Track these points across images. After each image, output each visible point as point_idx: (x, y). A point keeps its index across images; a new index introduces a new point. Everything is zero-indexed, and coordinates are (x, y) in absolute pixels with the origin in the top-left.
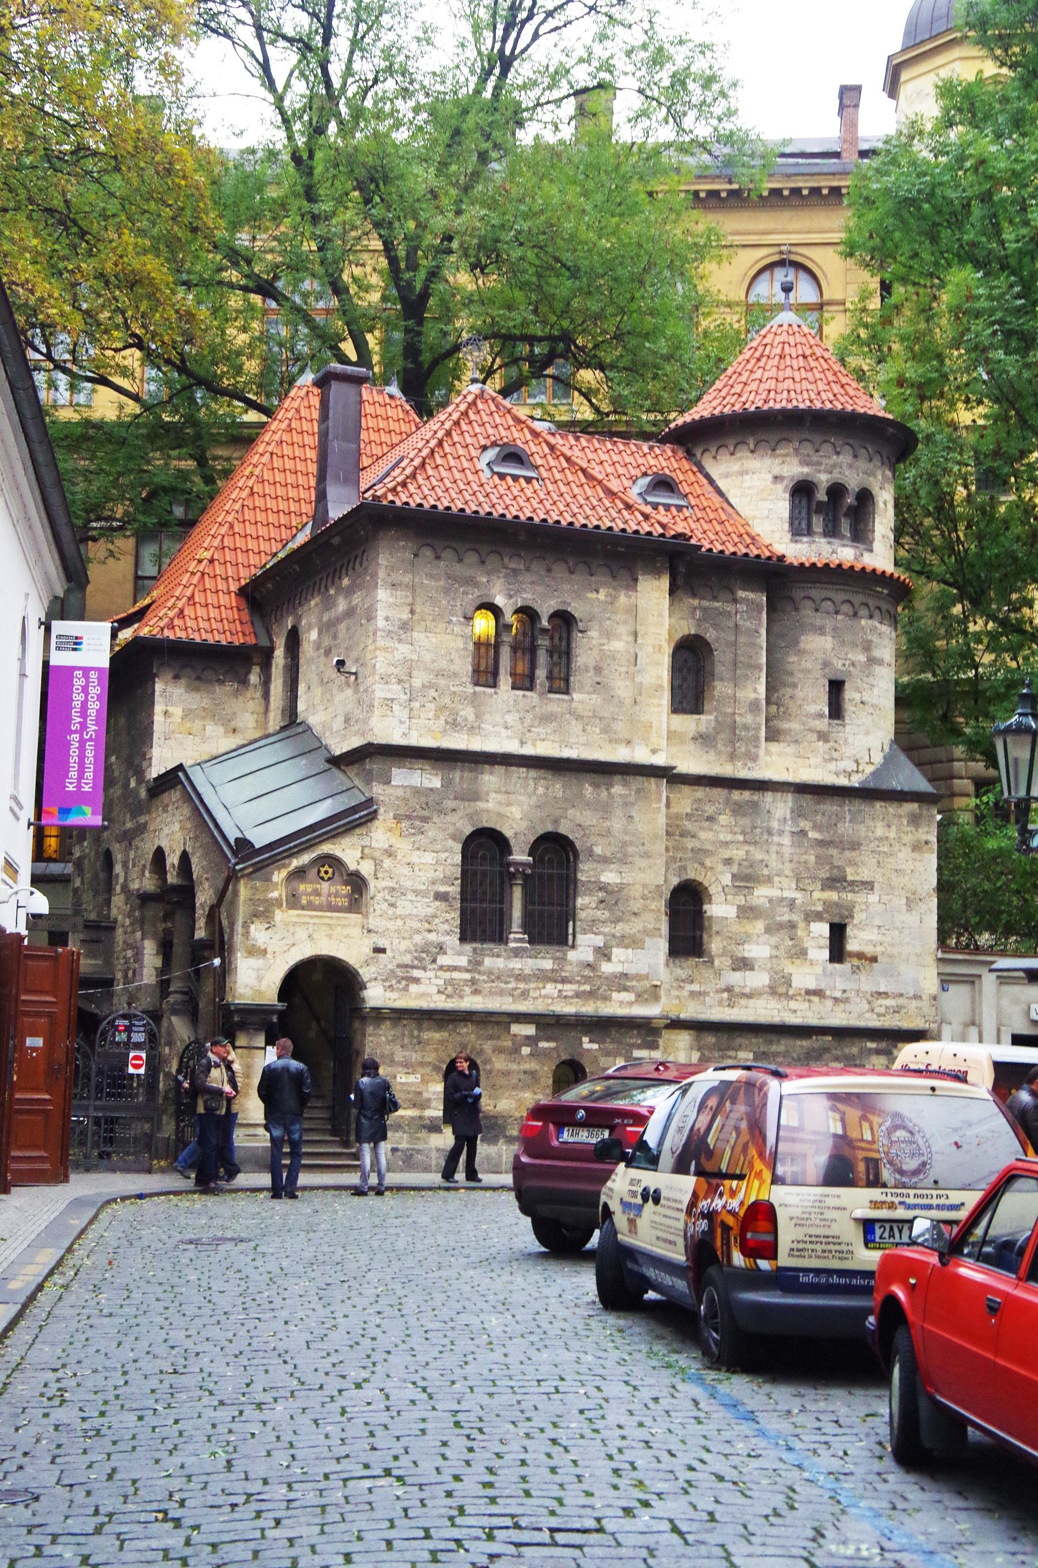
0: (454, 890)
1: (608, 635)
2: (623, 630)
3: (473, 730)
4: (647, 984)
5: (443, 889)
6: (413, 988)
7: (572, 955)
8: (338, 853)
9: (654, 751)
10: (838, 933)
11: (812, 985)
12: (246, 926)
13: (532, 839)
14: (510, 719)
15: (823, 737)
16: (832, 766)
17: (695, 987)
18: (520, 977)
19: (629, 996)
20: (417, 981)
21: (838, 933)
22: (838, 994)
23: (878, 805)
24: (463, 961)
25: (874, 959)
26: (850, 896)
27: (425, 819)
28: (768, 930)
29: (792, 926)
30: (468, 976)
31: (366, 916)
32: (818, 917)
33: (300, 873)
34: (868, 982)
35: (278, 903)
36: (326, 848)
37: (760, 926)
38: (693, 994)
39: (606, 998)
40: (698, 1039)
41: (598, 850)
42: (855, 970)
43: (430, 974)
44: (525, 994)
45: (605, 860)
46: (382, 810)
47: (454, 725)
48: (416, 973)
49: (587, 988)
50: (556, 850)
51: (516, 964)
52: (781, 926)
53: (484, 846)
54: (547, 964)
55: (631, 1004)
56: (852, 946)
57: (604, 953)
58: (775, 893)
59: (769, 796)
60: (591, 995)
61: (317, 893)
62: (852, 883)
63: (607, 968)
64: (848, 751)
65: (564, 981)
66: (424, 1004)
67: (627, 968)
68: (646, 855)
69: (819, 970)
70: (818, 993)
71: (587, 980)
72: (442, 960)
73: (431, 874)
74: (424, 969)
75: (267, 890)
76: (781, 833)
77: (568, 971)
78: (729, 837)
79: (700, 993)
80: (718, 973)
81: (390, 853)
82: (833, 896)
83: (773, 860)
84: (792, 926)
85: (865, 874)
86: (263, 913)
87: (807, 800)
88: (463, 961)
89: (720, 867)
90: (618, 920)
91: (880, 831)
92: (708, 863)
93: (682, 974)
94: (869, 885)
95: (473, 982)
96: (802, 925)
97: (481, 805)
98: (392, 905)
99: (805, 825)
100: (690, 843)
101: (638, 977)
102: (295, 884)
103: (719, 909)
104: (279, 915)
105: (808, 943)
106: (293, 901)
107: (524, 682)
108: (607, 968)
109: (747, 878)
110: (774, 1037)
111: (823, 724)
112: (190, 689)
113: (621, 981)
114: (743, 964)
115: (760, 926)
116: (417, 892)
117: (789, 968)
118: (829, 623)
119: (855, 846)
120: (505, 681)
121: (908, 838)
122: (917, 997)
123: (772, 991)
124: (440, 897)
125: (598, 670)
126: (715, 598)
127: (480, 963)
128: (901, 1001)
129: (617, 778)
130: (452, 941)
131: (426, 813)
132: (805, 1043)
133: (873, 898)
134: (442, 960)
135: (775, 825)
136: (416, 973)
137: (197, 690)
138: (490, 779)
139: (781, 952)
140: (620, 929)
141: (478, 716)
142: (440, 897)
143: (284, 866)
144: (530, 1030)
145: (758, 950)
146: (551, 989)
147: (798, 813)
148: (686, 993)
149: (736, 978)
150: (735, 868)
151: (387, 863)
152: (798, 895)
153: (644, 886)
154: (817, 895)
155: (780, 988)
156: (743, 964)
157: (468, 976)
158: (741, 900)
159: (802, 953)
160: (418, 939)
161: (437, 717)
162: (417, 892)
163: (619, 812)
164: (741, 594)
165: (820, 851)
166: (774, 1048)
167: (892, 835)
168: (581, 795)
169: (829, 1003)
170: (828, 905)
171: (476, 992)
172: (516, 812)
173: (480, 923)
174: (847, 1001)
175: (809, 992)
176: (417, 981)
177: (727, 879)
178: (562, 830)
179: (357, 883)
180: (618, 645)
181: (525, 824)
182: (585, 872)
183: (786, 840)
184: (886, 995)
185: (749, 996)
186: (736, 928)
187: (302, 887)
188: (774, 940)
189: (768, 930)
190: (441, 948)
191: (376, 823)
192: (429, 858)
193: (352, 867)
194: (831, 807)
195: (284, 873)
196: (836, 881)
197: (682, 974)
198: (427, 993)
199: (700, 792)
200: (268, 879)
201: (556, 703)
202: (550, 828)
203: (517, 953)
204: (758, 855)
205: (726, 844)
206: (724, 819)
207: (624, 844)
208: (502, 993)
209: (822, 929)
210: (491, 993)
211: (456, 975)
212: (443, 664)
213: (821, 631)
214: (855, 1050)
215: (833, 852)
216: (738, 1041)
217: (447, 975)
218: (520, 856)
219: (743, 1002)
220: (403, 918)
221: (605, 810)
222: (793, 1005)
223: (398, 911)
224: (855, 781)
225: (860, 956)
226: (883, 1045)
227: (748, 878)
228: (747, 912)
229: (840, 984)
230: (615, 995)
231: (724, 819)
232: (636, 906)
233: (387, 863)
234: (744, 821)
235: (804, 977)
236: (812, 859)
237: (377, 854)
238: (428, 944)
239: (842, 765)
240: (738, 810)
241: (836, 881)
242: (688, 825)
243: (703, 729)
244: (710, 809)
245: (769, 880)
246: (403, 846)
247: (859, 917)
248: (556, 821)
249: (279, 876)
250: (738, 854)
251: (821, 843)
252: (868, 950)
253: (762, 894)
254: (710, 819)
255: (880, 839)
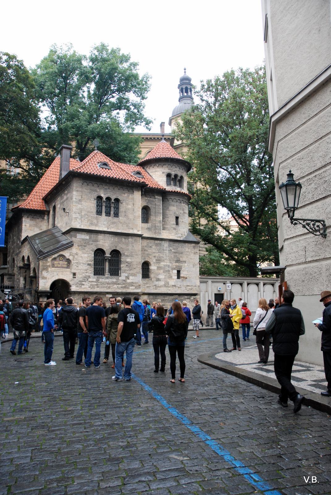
0: (92, 263)
1: (127, 204)
2: (131, 203)
3: (96, 225)
4: (138, 285)
5: (90, 263)
6: (83, 286)
7: (120, 278)
8: (64, 254)
9: (138, 231)
10: (179, 272)
11: (173, 284)
12: (41, 272)
13: (111, 251)
14: (105, 223)
15: (175, 229)
16: (177, 235)
17: (148, 285)
18: (108, 283)
19: (132, 287)
20: (83, 285)
21: (179, 272)
22: (179, 286)
23: (187, 244)
24: (95, 280)
25: (186, 278)
26: (181, 264)
27: (85, 246)
28: (164, 272)
29: (169, 271)
30: (96, 283)
31: (71, 269)
32: (174, 269)
33: (55, 259)
34: (185, 283)
35: (49, 266)
36: (61, 253)
37: (162, 271)
38: (148, 287)
39: (128, 288)
40: (149, 297)
41: (126, 254)
42: (183, 280)
43: (87, 283)
44: (109, 287)
45: (127, 256)
46: (74, 244)
47: (92, 224)
48: (83, 283)
49: (124, 286)
50: (116, 253)
51: (107, 280)
52: (167, 271)
53: (99, 252)
54: (115, 280)
55: (134, 289)
56: (182, 275)
57: (127, 278)
58: (166, 264)
59: (163, 242)
60: (125, 287)
61: (59, 264)
62: (182, 261)
63: (128, 281)
64: (180, 232)
65: (119, 284)
66: (85, 290)
67: (134, 281)
68: (137, 255)
69: (175, 281)
70: (175, 286)
71: (124, 284)
72: (90, 280)
73: (87, 259)
74: (85, 282)
75: (47, 263)
76: (166, 250)
77: (119, 282)
78: (155, 251)
79: (149, 287)
80: (153, 282)
81: (77, 254)
82: (177, 264)
83: (164, 256)
84: (169, 271)
85: (184, 260)
86: (46, 268)
87: (171, 243)
88: (95, 280)
89: (153, 258)
90: (131, 270)
91: (187, 250)
92: (150, 257)
93: (145, 282)
94: (185, 262)
95: (97, 285)
96: (171, 271)
97: (98, 243)
98: (77, 267)
99: (171, 248)
100: (146, 253)
101: (136, 283)
102: (53, 262)
103: (153, 267)
104: (49, 269)
105: (172, 275)
106: (53, 266)
107: (108, 214)
108: (128, 281)
109: (159, 261)
110: (165, 296)
111: (175, 226)
112: (31, 220)
113: (132, 284)
114: (158, 280)
115: (162, 271)
116: (83, 263)
117: (168, 280)
118: (175, 204)
119: (182, 253)
120: (104, 214)
121: (193, 251)
122: (195, 286)
123: (165, 286)
124: (89, 265)
125: (125, 212)
126: (151, 198)
127: (98, 280)
128: (192, 287)
129: (130, 237)
130: (92, 275)
131: (85, 245)
132: (172, 297)
133: (186, 265)
134: (90, 280)
135: (165, 248)
136: (83, 283)
137: (33, 220)
138: (101, 237)
139: (167, 277)
140: (131, 272)
141: (98, 222)
142: (89, 265)
143: (51, 257)
144: (111, 296)
145: (161, 277)
146: (115, 286)
147: (170, 246)
148: (146, 287)
149: (157, 283)
150: (156, 258)
151: (76, 257)
152: (170, 264)
153: (136, 262)
154: (174, 264)
155: (166, 285)
156: (158, 280)
157: (96, 283)
158: (158, 265)
159: (171, 277)
160: (84, 275)
161: (88, 222)
162: (83, 263)
163: (130, 245)
164: (156, 197)
165: (175, 254)
166: (165, 298)
167: (190, 251)
168: (121, 241)
169: (177, 288)
170: (177, 266)
171: (98, 287)
172: (107, 245)
173: (98, 271)
174: (181, 287)
175: (173, 286)
176: (83, 285)
177: (154, 261)
178: (117, 249)
179: (69, 261)
180: (130, 207)
181: (109, 247)
182: (123, 259)
183: (167, 252)
184: (188, 286)
185: (160, 287)
186: (157, 272)
187: (55, 262)
188: (165, 274)
189: (164, 272)
190: (89, 277)
191: (73, 247)
192: (86, 255)
193: (67, 257)
194: (177, 244)
195: (51, 259)
196: (178, 261)
197: (145, 282)
198: (86, 288)
199: (148, 241)
200: (47, 260)
201: (116, 219)
202: (115, 249)
203: (107, 278)
204: (161, 255)
205: (154, 253)
206: (154, 247)
207: (132, 252)
208: (104, 287)
209: (175, 272)
210: (101, 287)
211: (93, 283)
212: (89, 210)
213: (174, 206)
214: (183, 298)
215: (177, 254)
216: (158, 297)
217: (91, 283)
218: (108, 255)
219: (159, 288)
220: (80, 270)
221: (127, 244)
222: (169, 289)
223: (79, 268)
224: (182, 239)
225: (183, 277)
226: (188, 297)
227: (159, 260)
228: (159, 268)
229: (179, 284)
230: (130, 287)
231: (154, 247)
232: (135, 266)
233: (76, 257)
234: (158, 247)
235: (172, 283)
236: (173, 256)
237: (74, 254)
238: (86, 276)
239: (179, 235)
240: (157, 245)
241: (178, 261)
242: (146, 248)
243: (149, 227)
244: (150, 245)
245: (164, 261)
246: (80, 253)
247: (183, 269)
248: (116, 247)
249: (49, 260)
250: (157, 255)
251: (175, 252)
252: (185, 276)
253: (162, 264)
254: (150, 247)
255: (187, 252)
